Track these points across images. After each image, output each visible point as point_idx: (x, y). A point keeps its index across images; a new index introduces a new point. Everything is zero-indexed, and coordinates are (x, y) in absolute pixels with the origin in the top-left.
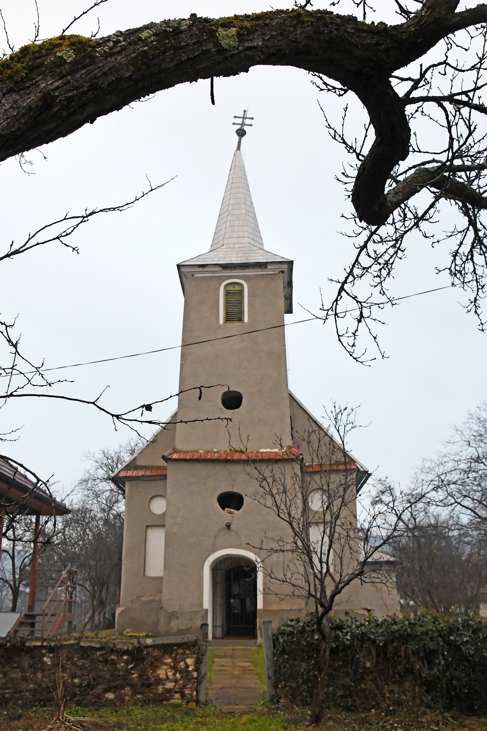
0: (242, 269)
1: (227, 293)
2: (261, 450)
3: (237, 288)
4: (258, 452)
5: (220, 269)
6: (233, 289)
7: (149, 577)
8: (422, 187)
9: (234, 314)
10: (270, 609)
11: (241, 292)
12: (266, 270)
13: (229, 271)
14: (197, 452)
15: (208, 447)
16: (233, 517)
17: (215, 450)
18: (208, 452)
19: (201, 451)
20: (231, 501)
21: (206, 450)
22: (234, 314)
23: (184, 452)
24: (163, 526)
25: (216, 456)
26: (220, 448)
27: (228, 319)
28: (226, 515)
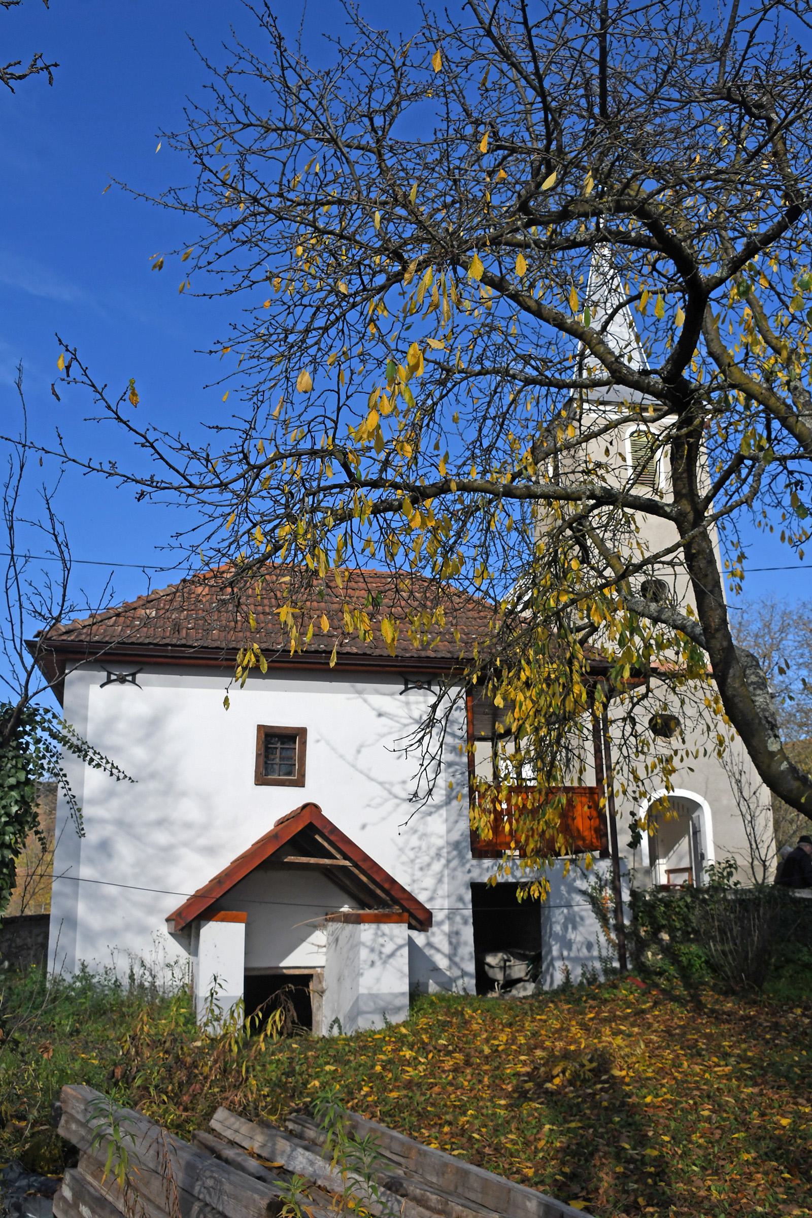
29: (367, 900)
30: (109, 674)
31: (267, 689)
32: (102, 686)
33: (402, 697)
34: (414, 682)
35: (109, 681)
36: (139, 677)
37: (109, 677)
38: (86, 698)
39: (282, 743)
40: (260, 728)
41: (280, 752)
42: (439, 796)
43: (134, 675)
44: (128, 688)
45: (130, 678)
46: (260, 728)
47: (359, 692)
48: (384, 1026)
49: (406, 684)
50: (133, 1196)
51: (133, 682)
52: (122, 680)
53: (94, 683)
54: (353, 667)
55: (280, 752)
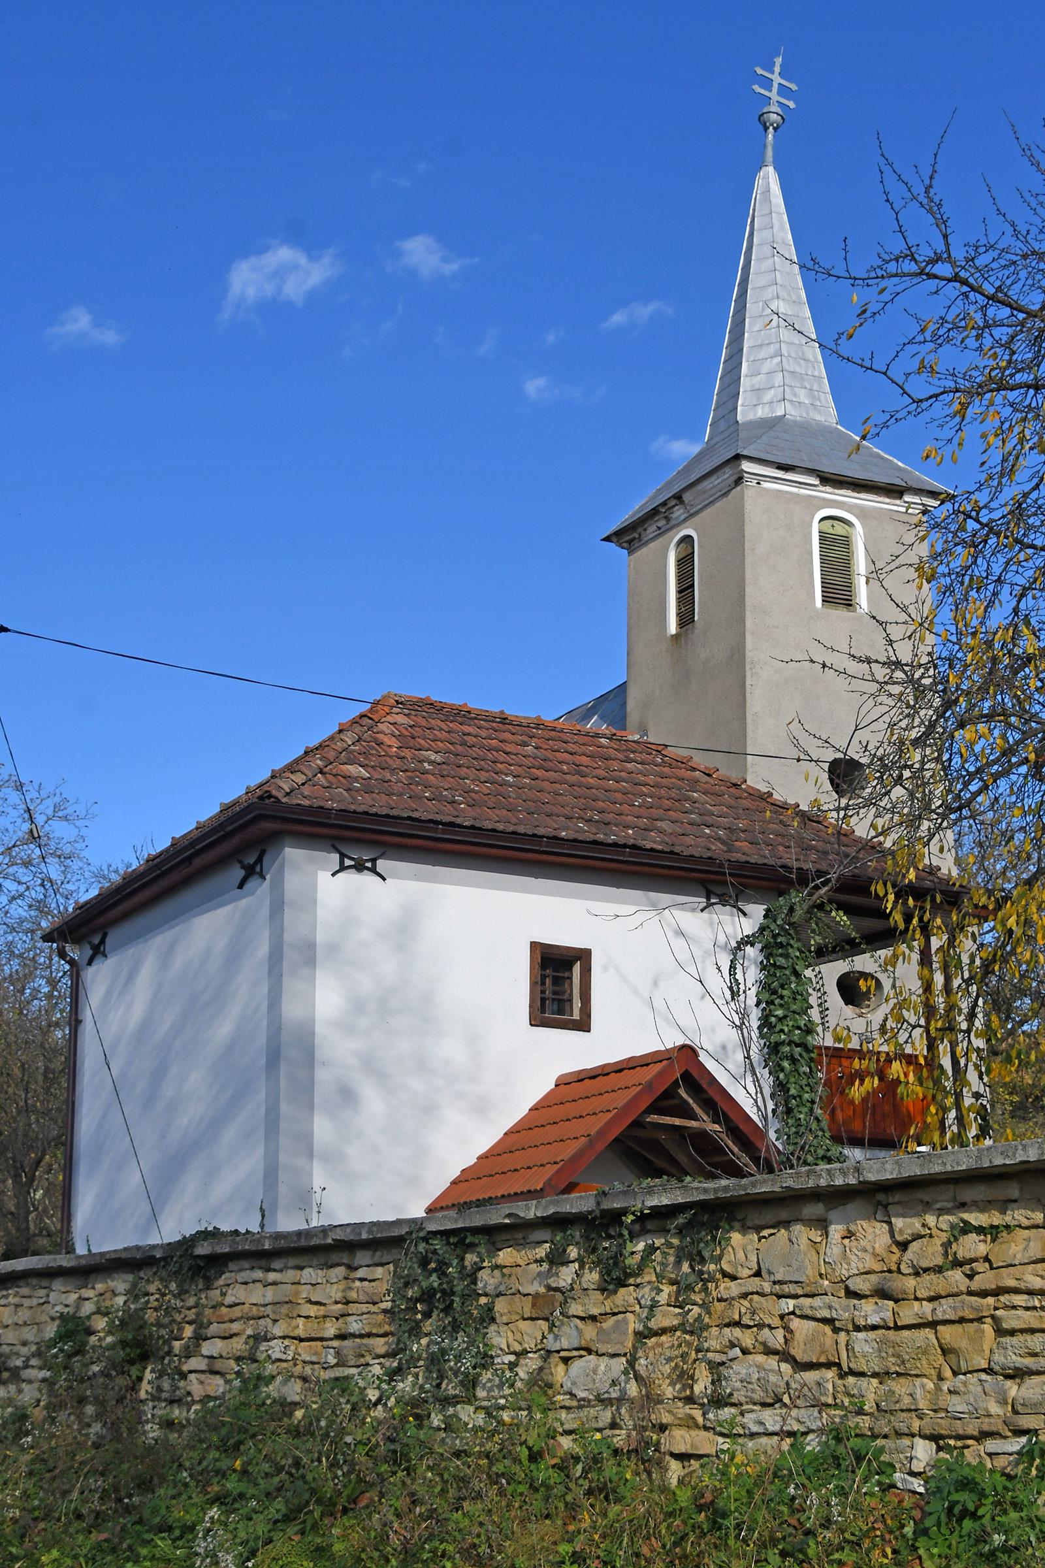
0: (853, 490)
1: (823, 537)
3: (840, 529)
5: (817, 482)
12: (898, 502)
13: (828, 489)
29: (659, 1163)
30: (343, 856)
31: (417, 877)
32: (333, 875)
33: (705, 915)
34: (718, 896)
35: (343, 868)
36: (381, 865)
37: (342, 862)
38: (314, 887)
39: (555, 970)
40: (534, 945)
41: (559, 983)
42: (1011, 1073)
43: (374, 861)
44: (368, 879)
45: (369, 865)
46: (534, 945)
47: (654, 906)
48: (86, 1253)
49: (708, 898)
50: (1016, 1448)
51: (373, 870)
52: (359, 867)
53: (323, 869)
54: (398, 839)
55: (559, 983)
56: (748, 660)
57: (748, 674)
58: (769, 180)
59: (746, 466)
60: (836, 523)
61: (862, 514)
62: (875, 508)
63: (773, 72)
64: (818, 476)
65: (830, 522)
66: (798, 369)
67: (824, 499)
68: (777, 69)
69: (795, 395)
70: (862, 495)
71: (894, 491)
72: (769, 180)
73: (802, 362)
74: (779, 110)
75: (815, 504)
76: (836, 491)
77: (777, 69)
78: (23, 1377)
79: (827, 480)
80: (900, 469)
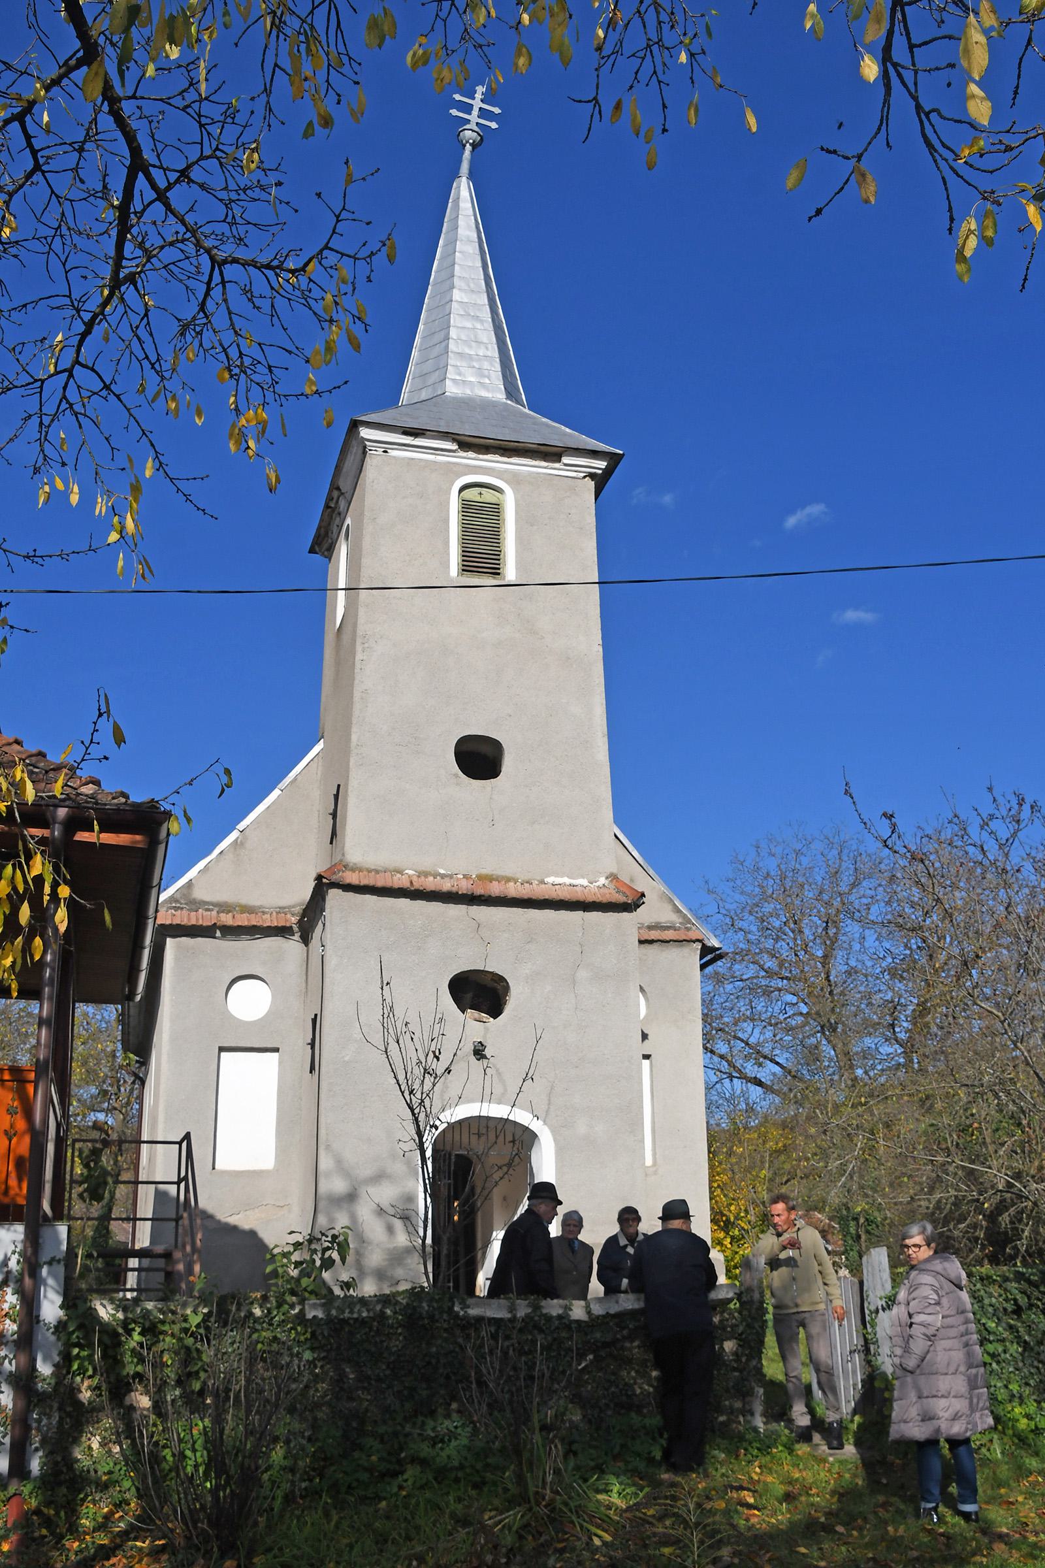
0: (502, 455)
1: (467, 507)
2: (550, 880)
3: (489, 496)
4: (542, 882)
5: (455, 447)
6: (478, 499)
7: (223, 1172)
8: (350, 452)
9: (481, 558)
10: (64, 1247)
11: (496, 510)
12: (557, 465)
13: (471, 454)
14: (401, 872)
15: (426, 864)
16: (487, 1029)
17: (442, 871)
18: (426, 874)
19: (411, 872)
20: (480, 992)
21: (422, 868)
22: (481, 558)
23: (369, 871)
24: (276, 1050)
25: (447, 886)
26: (455, 866)
27: (468, 566)
28: (471, 1026)
32: (641, 942)
56: (360, 632)
57: (359, 648)
58: (463, 192)
59: (365, 433)
60: (484, 490)
61: (515, 480)
62: (531, 473)
63: (474, 98)
64: (454, 440)
65: (478, 490)
66: (467, 351)
67: (467, 466)
68: (478, 96)
69: (460, 374)
70: (512, 460)
71: (551, 454)
72: (463, 192)
73: (474, 344)
74: (476, 129)
75: (454, 471)
76: (481, 456)
77: (478, 96)
78: (417, 1274)
79: (465, 444)
80: (565, 434)
